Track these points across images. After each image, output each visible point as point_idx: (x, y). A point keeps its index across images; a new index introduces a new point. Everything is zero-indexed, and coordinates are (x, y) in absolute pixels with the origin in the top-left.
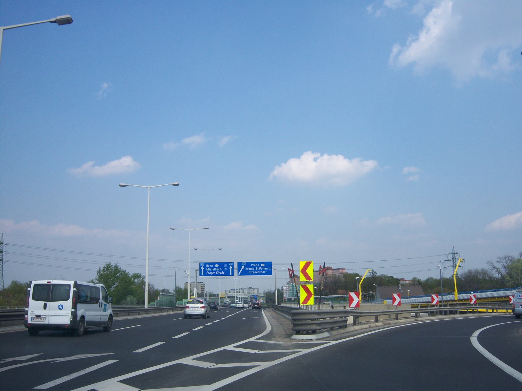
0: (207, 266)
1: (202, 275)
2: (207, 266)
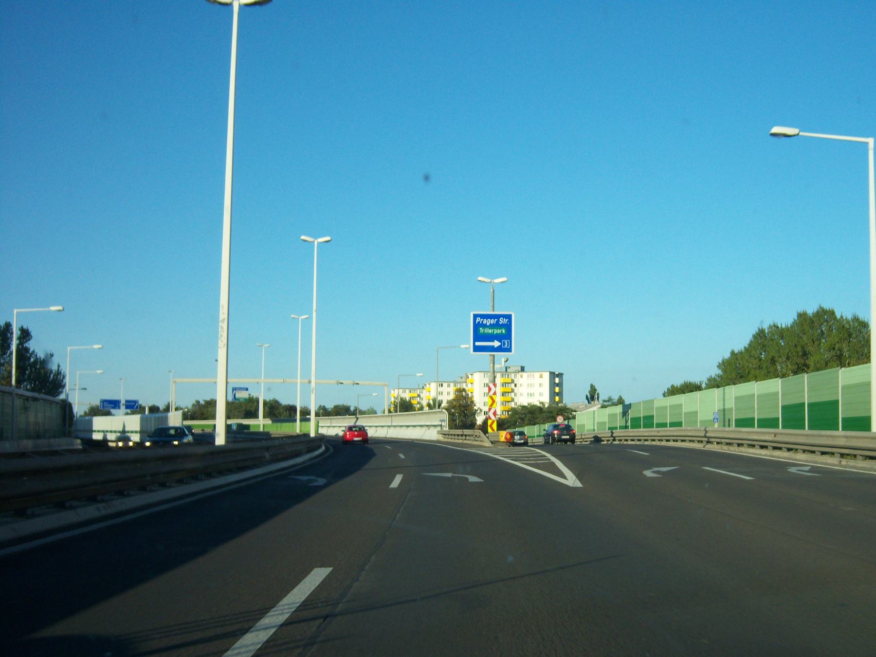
0: (105, 403)
1: (477, 344)
2: (105, 403)
